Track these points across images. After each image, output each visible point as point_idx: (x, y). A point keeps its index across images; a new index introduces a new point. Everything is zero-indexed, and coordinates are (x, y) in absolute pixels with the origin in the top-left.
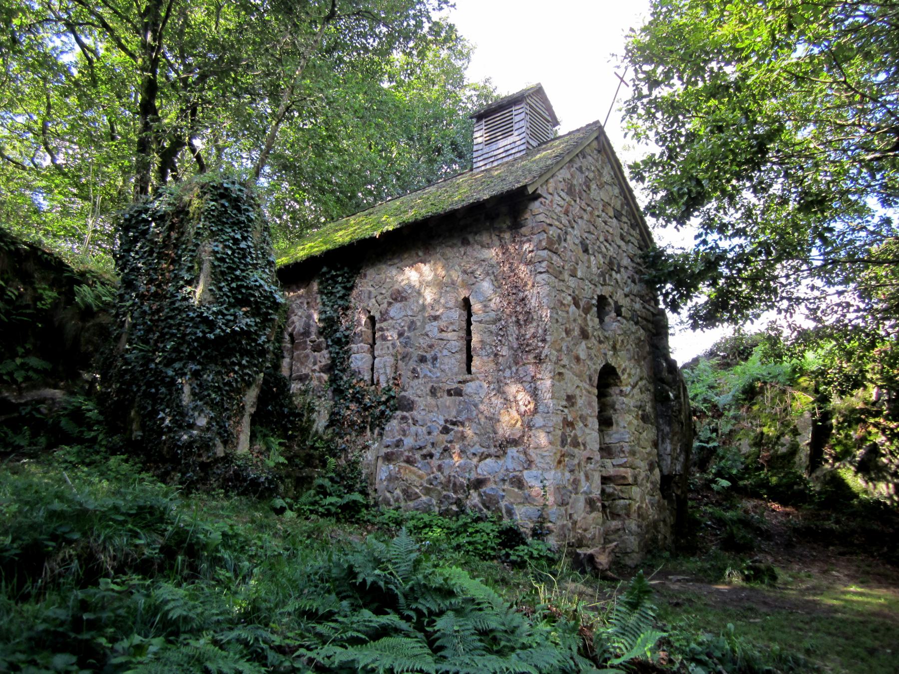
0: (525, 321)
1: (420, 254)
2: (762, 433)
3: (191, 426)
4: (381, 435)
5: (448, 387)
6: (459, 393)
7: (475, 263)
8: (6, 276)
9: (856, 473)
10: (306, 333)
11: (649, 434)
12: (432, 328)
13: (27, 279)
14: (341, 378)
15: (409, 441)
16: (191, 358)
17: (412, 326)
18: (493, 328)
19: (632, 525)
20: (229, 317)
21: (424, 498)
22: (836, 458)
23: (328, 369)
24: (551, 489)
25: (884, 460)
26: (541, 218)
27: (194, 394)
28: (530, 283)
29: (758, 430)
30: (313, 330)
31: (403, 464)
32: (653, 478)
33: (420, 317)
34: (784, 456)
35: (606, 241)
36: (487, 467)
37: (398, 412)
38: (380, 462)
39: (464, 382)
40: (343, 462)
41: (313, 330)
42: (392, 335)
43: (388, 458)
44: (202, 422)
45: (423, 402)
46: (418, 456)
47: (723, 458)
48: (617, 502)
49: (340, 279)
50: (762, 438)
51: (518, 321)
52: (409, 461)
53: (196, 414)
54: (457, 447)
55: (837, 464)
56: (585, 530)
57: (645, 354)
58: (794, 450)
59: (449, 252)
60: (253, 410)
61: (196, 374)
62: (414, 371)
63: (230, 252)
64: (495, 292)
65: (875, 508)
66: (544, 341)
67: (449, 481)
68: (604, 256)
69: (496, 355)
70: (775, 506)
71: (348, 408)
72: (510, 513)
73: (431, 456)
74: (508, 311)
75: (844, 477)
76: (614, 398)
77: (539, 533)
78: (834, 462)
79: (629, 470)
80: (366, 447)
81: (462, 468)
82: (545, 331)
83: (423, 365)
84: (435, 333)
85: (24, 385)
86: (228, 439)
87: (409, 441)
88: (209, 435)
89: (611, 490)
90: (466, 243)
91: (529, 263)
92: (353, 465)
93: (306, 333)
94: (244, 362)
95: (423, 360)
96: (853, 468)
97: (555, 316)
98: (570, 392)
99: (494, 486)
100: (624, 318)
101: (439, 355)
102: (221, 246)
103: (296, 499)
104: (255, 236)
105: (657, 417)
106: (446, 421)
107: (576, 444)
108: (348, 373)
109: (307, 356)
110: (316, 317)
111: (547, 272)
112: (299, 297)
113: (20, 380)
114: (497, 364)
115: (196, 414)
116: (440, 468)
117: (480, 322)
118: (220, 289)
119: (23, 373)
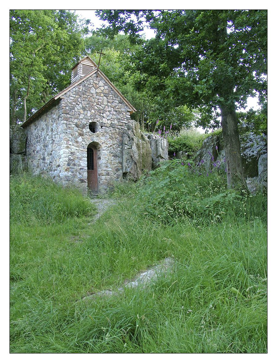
6: (51, 154)
26: (63, 105)
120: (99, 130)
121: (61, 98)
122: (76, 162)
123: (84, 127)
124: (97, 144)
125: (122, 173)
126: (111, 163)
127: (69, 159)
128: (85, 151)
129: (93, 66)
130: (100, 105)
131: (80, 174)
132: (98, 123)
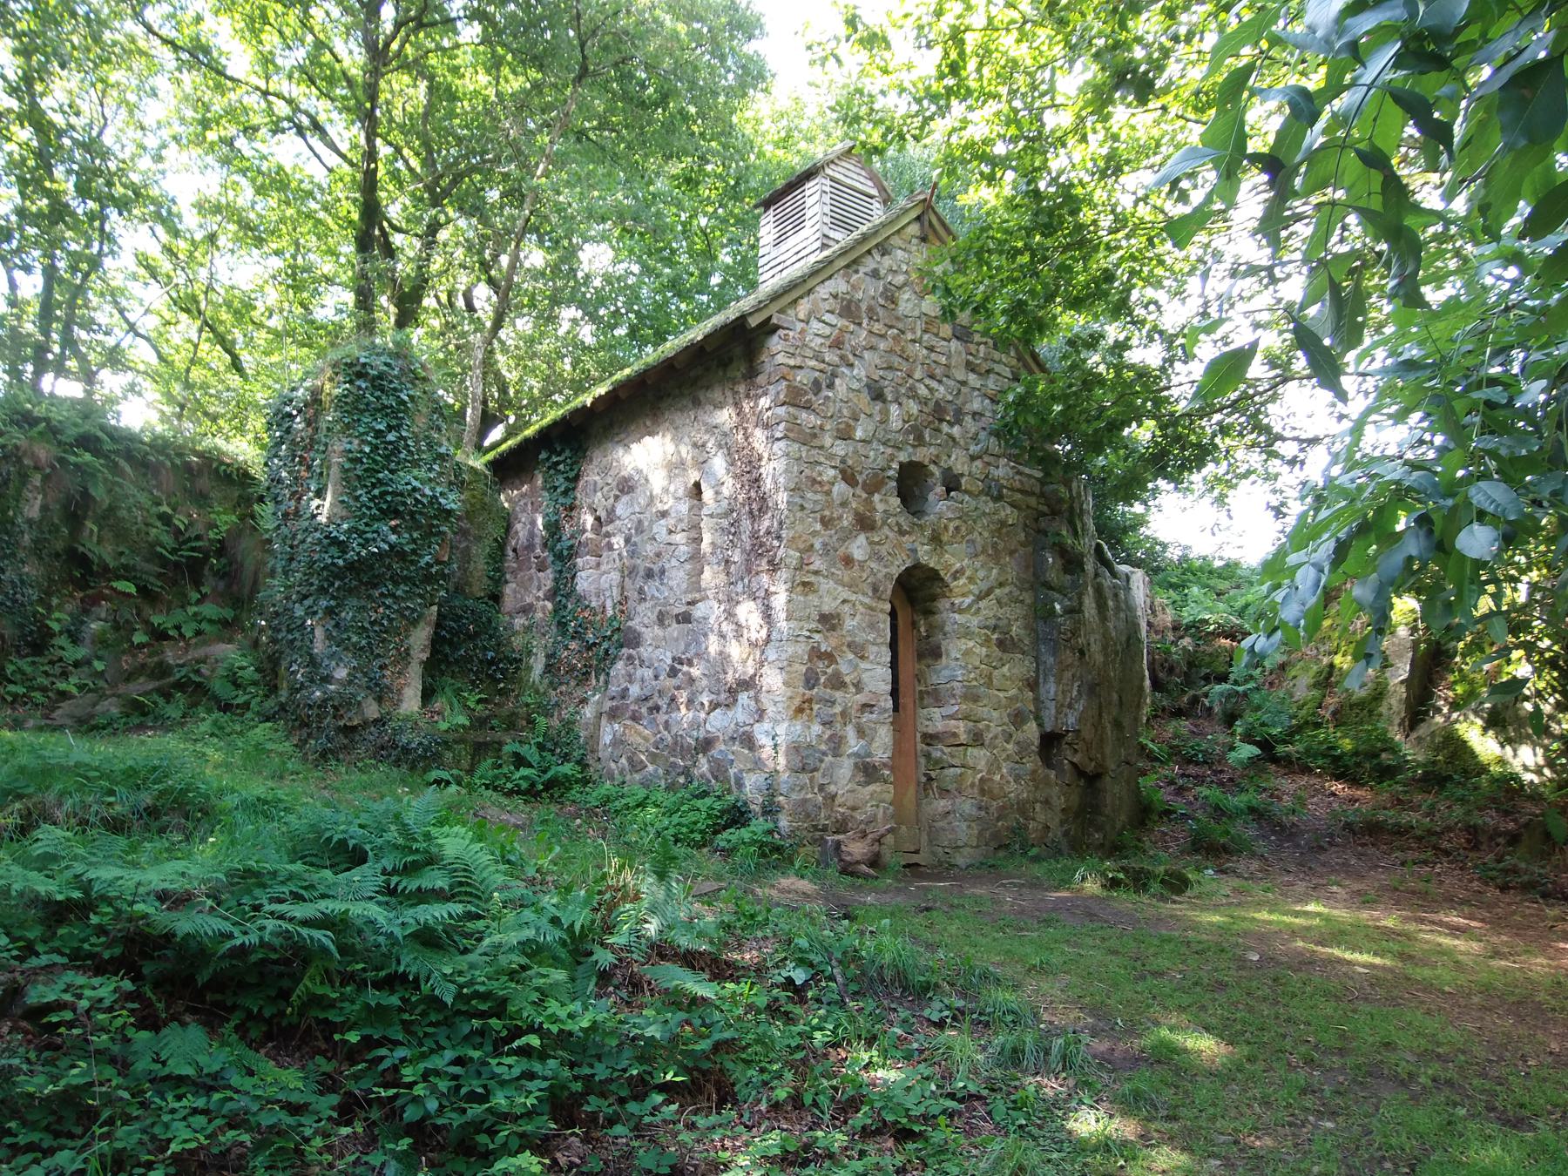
0: (760, 510)
1: (648, 423)
2: (1332, 666)
3: (327, 679)
4: (607, 682)
5: (676, 611)
6: (685, 618)
7: (707, 431)
8: (173, 500)
9: (1485, 730)
10: (530, 547)
11: (1015, 669)
12: (660, 529)
13: (201, 499)
14: (565, 607)
15: (635, 690)
16: (322, 590)
17: (639, 527)
18: (725, 523)
19: (967, 807)
20: (369, 536)
21: (651, 768)
22: (1454, 706)
23: (552, 595)
24: (782, 749)
25: (1528, 706)
26: (780, 359)
27: (329, 637)
28: (766, 455)
29: (1325, 660)
30: (538, 540)
31: (628, 722)
32: (1018, 736)
33: (648, 515)
34: (1361, 704)
35: (932, 377)
36: (718, 722)
37: (624, 650)
38: (604, 721)
39: (692, 603)
40: (555, 722)
41: (538, 540)
42: (619, 541)
43: (614, 715)
44: (341, 673)
45: (650, 633)
46: (644, 710)
47: (1258, 708)
48: (946, 771)
49: (561, 467)
50: (1330, 674)
51: (751, 512)
52: (635, 718)
53: (333, 663)
54: (683, 697)
55: (1455, 715)
56: (854, 809)
57: (1013, 545)
58: (1379, 694)
59: (679, 418)
60: (424, 656)
61: (330, 612)
62: (641, 591)
63: (367, 449)
64: (728, 471)
65: (1509, 786)
66: (779, 538)
67: (676, 743)
68: (924, 402)
69: (727, 562)
70: (1337, 787)
71: (567, 648)
72: (740, 784)
73: (657, 708)
74: (740, 498)
75: (1466, 737)
76: (944, 615)
77: (770, 810)
78: (1450, 712)
79: (961, 723)
80: (584, 701)
81: (695, 725)
82: (781, 523)
83: (650, 582)
84: (662, 535)
85: (194, 641)
86: (381, 693)
87: (635, 690)
88: (350, 690)
89: (939, 754)
90: (697, 403)
91: (767, 426)
92: (568, 725)
93: (530, 547)
94: (399, 593)
95: (649, 574)
96: (1479, 722)
97: (798, 500)
98: (826, 609)
99: (723, 747)
100: (966, 492)
101: (667, 566)
102: (356, 442)
103: (471, 771)
104: (419, 423)
105: (1036, 642)
106: (674, 659)
107: (837, 683)
108: (573, 599)
109: (531, 579)
110: (540, 521)
111: (785, 437)
112: (523, 496)
113: (188, 634)
114: (728, 574)
115: (333, 663)
116: (667, 725)
117: (711, 516)
118: (357, 499)
119: (194, 625)
120: (939, 506)
121: (774, 321)
122: (844, 668)
123: (873, 486)
124: (933, 576)
125: (1037, 735)
126: (990, 677)
127: (816, 654)
128: (882, 611)
129: (874, 192)
130: (940, 382)
131: (861, 733)
132: (932, 467)
